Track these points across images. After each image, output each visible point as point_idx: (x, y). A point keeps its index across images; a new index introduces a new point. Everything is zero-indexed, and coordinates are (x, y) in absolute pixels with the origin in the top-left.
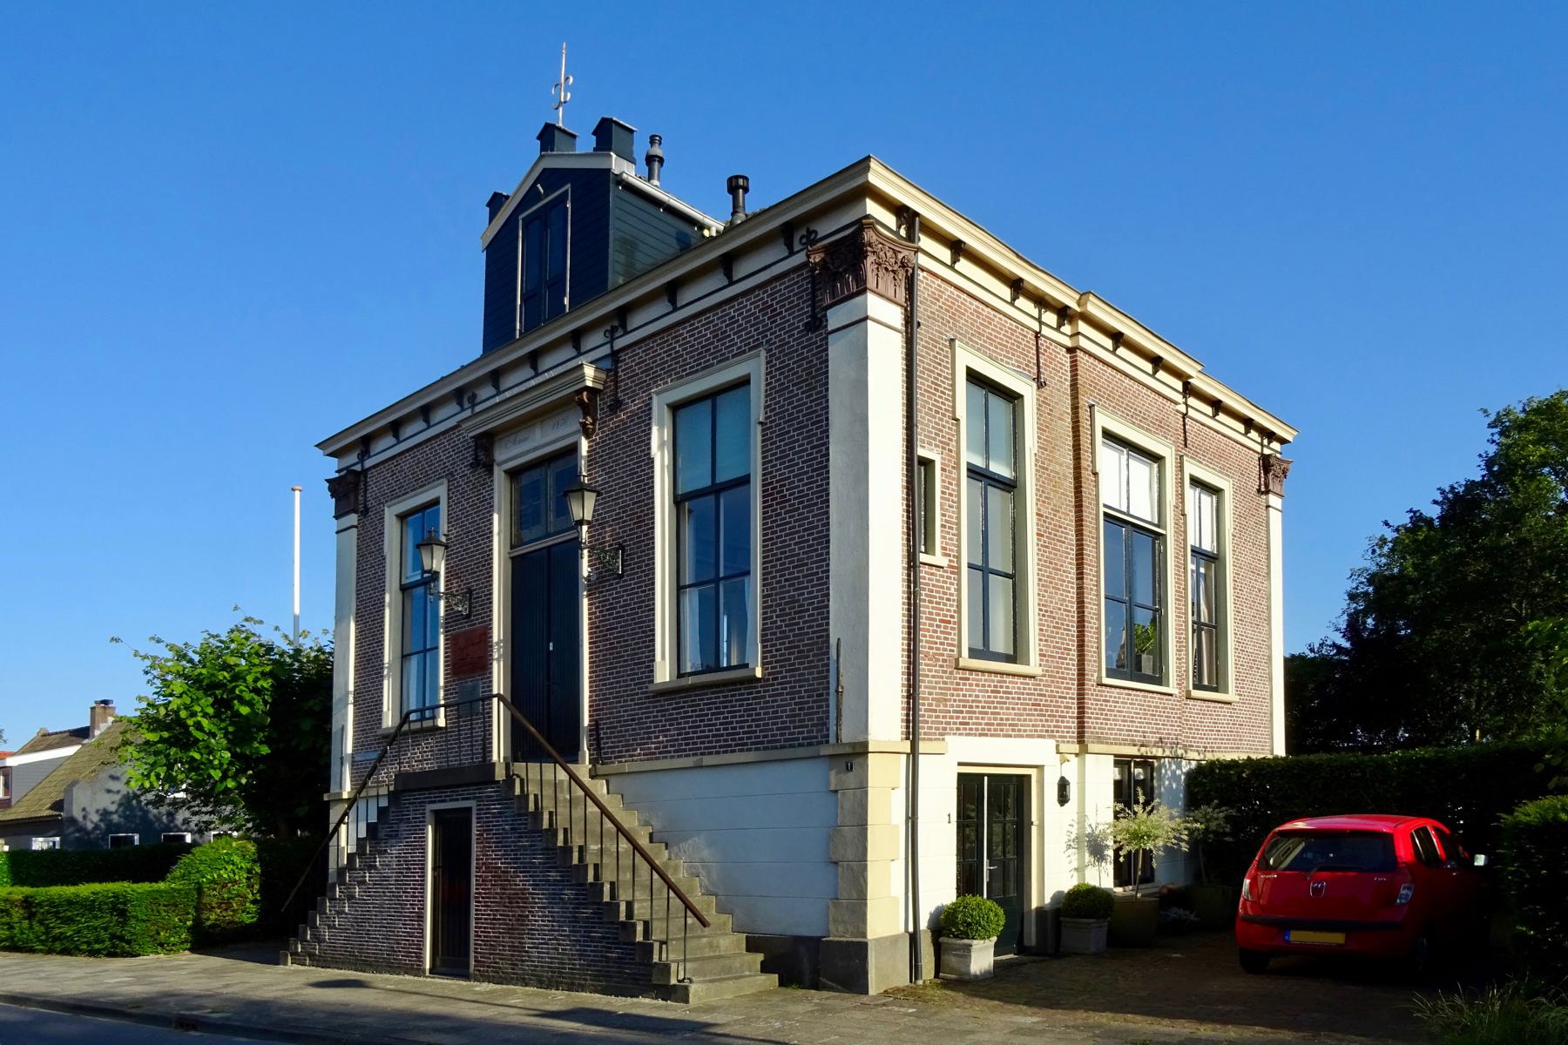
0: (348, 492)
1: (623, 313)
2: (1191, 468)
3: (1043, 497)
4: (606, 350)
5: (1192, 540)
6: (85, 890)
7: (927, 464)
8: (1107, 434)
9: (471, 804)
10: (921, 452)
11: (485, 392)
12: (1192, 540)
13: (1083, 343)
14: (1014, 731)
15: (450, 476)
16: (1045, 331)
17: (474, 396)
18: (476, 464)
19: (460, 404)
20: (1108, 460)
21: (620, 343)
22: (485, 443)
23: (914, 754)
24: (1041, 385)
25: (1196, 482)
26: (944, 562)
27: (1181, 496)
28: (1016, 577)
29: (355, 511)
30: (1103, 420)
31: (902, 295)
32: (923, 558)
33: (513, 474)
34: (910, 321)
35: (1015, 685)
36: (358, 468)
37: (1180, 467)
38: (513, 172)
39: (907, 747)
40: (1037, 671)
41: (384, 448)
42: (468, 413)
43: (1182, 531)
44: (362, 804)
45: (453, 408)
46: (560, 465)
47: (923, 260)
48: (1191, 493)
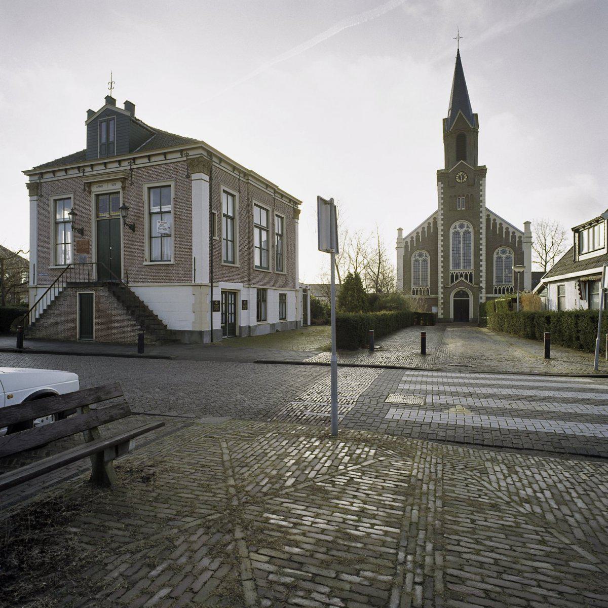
0: (34, 188)
1: (134, 159)
2: (276, 213)
3: (240, 222)
4: (129, 168)
5: (276, 231)
6: (78, 304)
7: (214, 214)
8: (255, 204)
9: (94, 292)
10: (213, 211)
11: (89, 169)
12: (276, 231)
13: (250, 181)
14: (233, 281)
15: (75, 192)
16: (241, 178)
17: (84, 170)
18: (84, 190)
19: (79, 171)
20: (256, 210)
21: (133, 167)
22: (90, 184)
23: (212, 286)
24: (240, 193)
25: (277, 215)
26: (218, 239)
27: (273, 220)
28: (233, 242)
29: (37, 195)
30: (254, 202)
31: (209, 174)
32: (214, 238)
33: (97, 196)
34: (210, 179)
35: (234, 270)
36: (38, 181)
37: (273, 212)
38: (98, 105)
39: (210, 284)
40: (239, 266)
41: (48, 177)
42: (82, 174)
43: (273, 229)
44: (52, 289)
45: (76, 171)
46: (115, 196)
47: (213, 163)
48: (276, 218)
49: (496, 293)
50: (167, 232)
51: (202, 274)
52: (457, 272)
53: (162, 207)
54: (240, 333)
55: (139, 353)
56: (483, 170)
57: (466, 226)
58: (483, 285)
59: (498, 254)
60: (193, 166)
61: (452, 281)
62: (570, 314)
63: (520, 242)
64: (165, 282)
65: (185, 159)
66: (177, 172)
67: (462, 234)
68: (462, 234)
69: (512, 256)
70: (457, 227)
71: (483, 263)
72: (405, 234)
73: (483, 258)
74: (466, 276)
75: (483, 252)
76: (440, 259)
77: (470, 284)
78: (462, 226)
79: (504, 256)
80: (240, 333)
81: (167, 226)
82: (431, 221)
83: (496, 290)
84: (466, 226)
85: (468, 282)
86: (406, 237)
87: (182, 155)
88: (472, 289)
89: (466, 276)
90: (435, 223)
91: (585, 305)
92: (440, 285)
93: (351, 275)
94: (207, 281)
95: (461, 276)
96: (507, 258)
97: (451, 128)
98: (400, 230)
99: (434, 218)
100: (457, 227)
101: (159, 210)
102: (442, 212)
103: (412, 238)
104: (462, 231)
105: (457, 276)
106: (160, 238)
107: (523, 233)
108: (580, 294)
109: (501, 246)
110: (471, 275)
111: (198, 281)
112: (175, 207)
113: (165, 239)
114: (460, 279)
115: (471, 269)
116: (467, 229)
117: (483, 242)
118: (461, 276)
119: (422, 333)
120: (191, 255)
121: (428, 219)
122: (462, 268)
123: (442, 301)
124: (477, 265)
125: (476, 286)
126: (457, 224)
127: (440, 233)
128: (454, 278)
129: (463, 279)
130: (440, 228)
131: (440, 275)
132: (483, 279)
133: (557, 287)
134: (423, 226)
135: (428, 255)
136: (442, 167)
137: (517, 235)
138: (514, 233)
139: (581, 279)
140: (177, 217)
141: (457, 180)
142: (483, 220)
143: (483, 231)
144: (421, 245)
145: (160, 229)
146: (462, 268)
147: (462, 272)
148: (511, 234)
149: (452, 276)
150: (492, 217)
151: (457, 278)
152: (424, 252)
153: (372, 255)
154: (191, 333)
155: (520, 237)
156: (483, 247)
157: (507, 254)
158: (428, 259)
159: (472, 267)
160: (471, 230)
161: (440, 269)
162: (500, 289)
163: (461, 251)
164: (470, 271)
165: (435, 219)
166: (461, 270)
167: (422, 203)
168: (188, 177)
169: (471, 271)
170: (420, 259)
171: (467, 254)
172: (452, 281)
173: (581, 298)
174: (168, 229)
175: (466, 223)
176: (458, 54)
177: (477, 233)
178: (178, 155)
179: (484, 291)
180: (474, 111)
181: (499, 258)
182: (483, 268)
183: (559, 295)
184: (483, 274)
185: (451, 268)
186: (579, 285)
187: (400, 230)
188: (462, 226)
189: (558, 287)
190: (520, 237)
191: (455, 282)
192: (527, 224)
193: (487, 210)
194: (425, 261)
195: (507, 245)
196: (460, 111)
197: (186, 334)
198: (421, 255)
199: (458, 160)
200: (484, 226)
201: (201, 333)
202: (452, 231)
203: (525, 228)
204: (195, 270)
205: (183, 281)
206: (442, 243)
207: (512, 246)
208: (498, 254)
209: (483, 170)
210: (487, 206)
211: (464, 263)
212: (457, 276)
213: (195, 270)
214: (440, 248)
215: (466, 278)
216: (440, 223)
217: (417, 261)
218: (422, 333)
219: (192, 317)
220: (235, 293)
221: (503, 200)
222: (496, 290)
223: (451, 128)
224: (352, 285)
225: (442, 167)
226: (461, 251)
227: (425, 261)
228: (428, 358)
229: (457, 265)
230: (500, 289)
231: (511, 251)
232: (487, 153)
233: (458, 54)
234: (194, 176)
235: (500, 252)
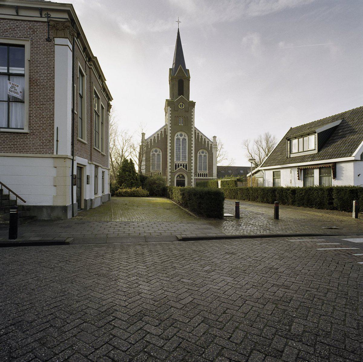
49: (199, 176)
50: (19, 96)
51: (64, 147)
52: (179, 163)
53: (10, 68)
54: (86, 206)
55: (10, 238)
56: (193, 104)
57: (183, 135)
58: (193, 171)
59: (200, 153)
60: (57, 29)
61: (176, 169)
62: (282, 189)
63: (211, 147)
64: (33, 152)
65: (45, 20)
66: (34, 32)
67: (181, 140)
68: (181, 140)
69: (207, 155)
70: (179, 135)
71: (193, 158)
72: (146, 137)
73: (193, 155)
74: (184, 165)
75: (193, 152)
76: (169, 154)
77: (186, 170)
78: (181, 135)
79: (203, 155)
80: (86, 206)
81: (19, 89)
82: (163, 130)
83: (199, 174)
84: (183, 135)
85: (184, 169)
86: (148, 139)
87: (41, 14)
88: (187, 173)
89: (184, 165)
90: (165, 131)
91: (300, 184)
92: (169, 170)
93: (127, 160)
94: (69, 154)
95: (181, 165)
96: (205, 156)
97: (175, 75)
98: (143, 134)
99: (165, 129)
100: (179, 135)
101: (6, 71)
102: (170, 125)
103: (151, 140)
104: (181, 138)
105: (178, 165)
106: (5, 104)
107: (213, 143)
108: (298, 176)
109: (201, 149)
110: (186, 165)
111: (60, 153)
112: (30, 70)
113: (13, 106)
114: (180, 167)
115: (186, 162)
116: (184, 137)
117: (193, 145)
118: (181, 165)
119: (236, 203)
120: (52, 125)
121: (161, 129)
122: (181, 161)
123: (170, 181)
124: (190, 160)
125: (189, 172)
126: (179, 133)
127: (169, 138)
128: (177, 166)
129: (182, 167)
130: (169, 135)
131: (169, 164)
132: (193, 168)
133: (272, 173)
134: (157, 133)
135: (161, 152)
136: (169, 98)
137: (210, 143)
138: (208, 142)
139: (301, 168)
140: (32, 81)
141: (179, 107)
142: (193, 133)
143: (193, 139)
144: (153, 146)
145: (11, 91)
146: (181, 161)
147: (181, 163)
148: (207, 143)
149: (176, 165)
150: (197, 132)
151: (178, 167)
152: (158, 150)
153: (357, 128)
154: (52, 208)
155: (211, 145)
156: (193, 149)
157: (205, 154)
158: (161, 154)
159: (187, 160)
160: (187, 138)
161: (169, 161)
162: (201, 174)
163: (181, 151)
164: (186, 163)
165: (165, 129)
166: (181, 162)
167: (156, 120)
168: (49, 40)
169: (186, 163)
170: (156, 154)
171: (184, 152)
172: (176, 169)
173: (299, 179)
174: (19, 93)
175: (183, 134)
176: (178, 30)
177: (190, 140)
178: (37, 14)
179: (193, 174)
180: (187, 68)
181: (201, 156)
182: (193, 161)
183: (274, 176)
184: (193, 165)
185: (175, 160)
186: (298, 171)
187: (143, 134)
188: (181, 135)
189: (273, 172)
190: (211, 145)
191: (178, 169)
192: (215, 137)
193: (195, 127)
194: (158, 155)
195: (205, 149)
196: (180, 66)
197: (45, 210)
198: (156, 151)
199: (179, 95)
200: (193, 136)
201: (65, 208)
202: (176, 138)
203: (214, 139)
204: (57, 141)
205: (40, 152)
206: (170, 145)
207: (207, 149)
208: (200, 153)
209: (193, 104)
210: (195, 126)
211: (182, 157)
212: (178, 165)
213: (57, 141)
214: (169, 148)
215: (184, 167)
216: (169, 132)
217: (154, 155)
218: (236, 203)
219: (53, 191)
220: (81, 168)
221: (203, 122)
222: (199, 174)
223: (175, 75)
224: (129, 168)
225: (169, 98)
226: (181, 151)
227: (158, 155)
228: (280, 223)
229: (178, 159)
230: (201, 174)
231: (207, 152)
232: (196, 92)
233: (178, 30)
234: (57, 41)
235: (201, 152)
